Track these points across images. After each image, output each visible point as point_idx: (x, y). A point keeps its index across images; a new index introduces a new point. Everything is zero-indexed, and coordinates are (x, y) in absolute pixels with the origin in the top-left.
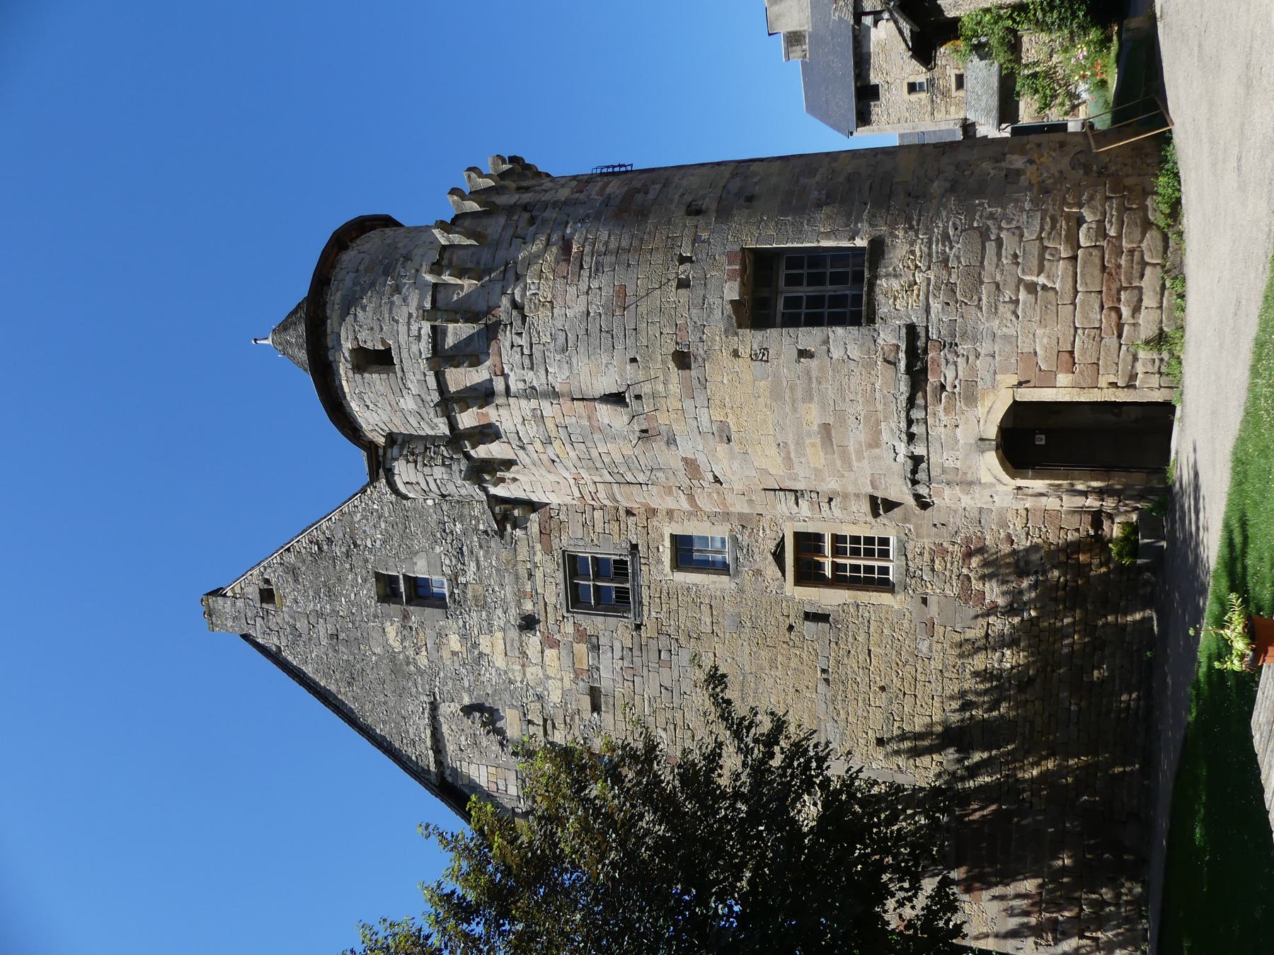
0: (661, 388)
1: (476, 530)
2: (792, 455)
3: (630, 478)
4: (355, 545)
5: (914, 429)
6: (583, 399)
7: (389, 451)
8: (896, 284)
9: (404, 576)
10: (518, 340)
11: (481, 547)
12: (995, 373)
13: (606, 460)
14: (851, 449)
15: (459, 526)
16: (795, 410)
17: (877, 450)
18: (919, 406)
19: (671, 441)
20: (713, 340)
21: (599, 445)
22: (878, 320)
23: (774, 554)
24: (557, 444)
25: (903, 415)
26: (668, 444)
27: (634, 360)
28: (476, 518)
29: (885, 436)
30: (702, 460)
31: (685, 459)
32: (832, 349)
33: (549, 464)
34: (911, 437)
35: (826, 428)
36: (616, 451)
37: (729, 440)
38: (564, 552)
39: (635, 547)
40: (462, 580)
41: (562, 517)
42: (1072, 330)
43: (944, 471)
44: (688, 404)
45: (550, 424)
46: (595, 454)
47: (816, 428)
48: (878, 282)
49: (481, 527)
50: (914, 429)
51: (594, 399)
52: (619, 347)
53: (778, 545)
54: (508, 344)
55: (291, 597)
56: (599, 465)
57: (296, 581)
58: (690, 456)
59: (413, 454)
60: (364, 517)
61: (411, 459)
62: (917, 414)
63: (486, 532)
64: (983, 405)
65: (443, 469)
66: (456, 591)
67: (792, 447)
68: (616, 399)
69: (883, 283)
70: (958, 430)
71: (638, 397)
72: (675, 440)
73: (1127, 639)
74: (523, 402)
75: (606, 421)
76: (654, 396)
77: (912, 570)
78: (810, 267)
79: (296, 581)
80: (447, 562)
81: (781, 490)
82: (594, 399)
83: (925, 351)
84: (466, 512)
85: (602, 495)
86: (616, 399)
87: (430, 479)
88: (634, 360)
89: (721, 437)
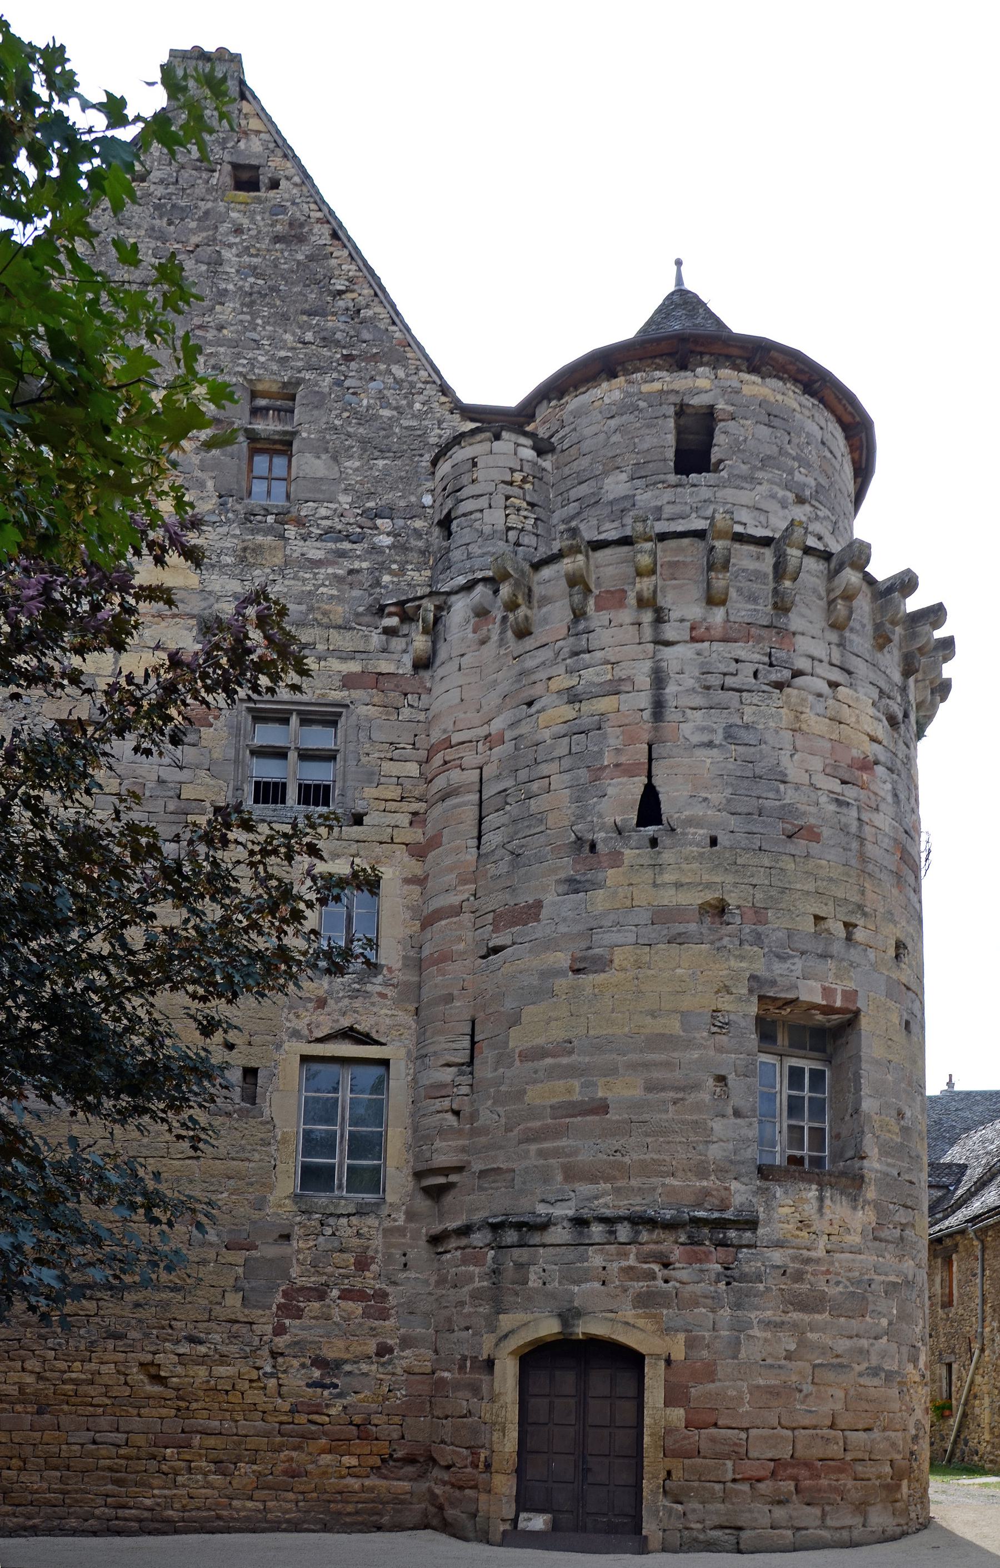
0: (668, 877)
1: (382, 567)
2: (549, 1061)
3: (492, 820)
4: (348, 358)
5: (597, 1230)
6: (650, 760)
7: (529, 442)
8: (810, 1209)
9: (294, 434)
10: (748, 669)
11: (351, 572)
12: (686, 1331)
13: (535, 787)
14: (563, 1142)
15: (386, 541)
16: (634, 1067)
17: (560, 1178)
18: (638, 1233)
19: (574, 886)
20: (742, 958)
21: (566, 777)
22: (765, 1184)
23: (351, 1028)
24: (568, 712)
25: (622, 1212)
26: (570, 881)
27: (714, 842)
28: (402, 571)
29: (585, 1189)
30: (538, 930)
31: (539, 904)
32: (725, 1121)
33: (527, 694)
34: (580, 1222)
35: (602, 1108)
36: (557, 802)
37: (577, 971)
38: (347, 706)
39: (358, 820)
40: (291, 531)
41: (406, 713)
42: (745, 1425)
43: (520, 1266)
44: (644, 917)
45: (605, 704)
46: (545, 769)
47: (600, 1094)
48: (814, 1187)
49: (386, 578)
50: (597, 1230)
51: (650, 776)
52: (733, 821)
53: (367, 1035)
54: (742, 654)
55: (246, 223)
56: (523, 775)
57: (277, 239)
58: (544, 913)
59: (524, 480)
60: (398, 382)
61: (518, 476)
62: (623, 1232)
63: (378, 583)
64: (638, 1316)
65: (500, 526)
66: (270, 519)
67: (565, 1060)
68: (650, 808)
69: (812, 1193)
70: (597, 1285)
71: (654, 842)
72: (577, 891)
73: (235, 1503)
74: (647, 666)
75: (610, 791)
76: (657, 867)
77: (331, 1221)
78: (810, 1098)
79: (277, 239)
80: (323, 512)
81: (473, 1043)
82: (650, 776)
83: (723, 1244)
84: (413, 556)
85: (456, 776)
86: (650, 808)
87: (483, 502)
88: (714, 842)
89: (584, 959)
